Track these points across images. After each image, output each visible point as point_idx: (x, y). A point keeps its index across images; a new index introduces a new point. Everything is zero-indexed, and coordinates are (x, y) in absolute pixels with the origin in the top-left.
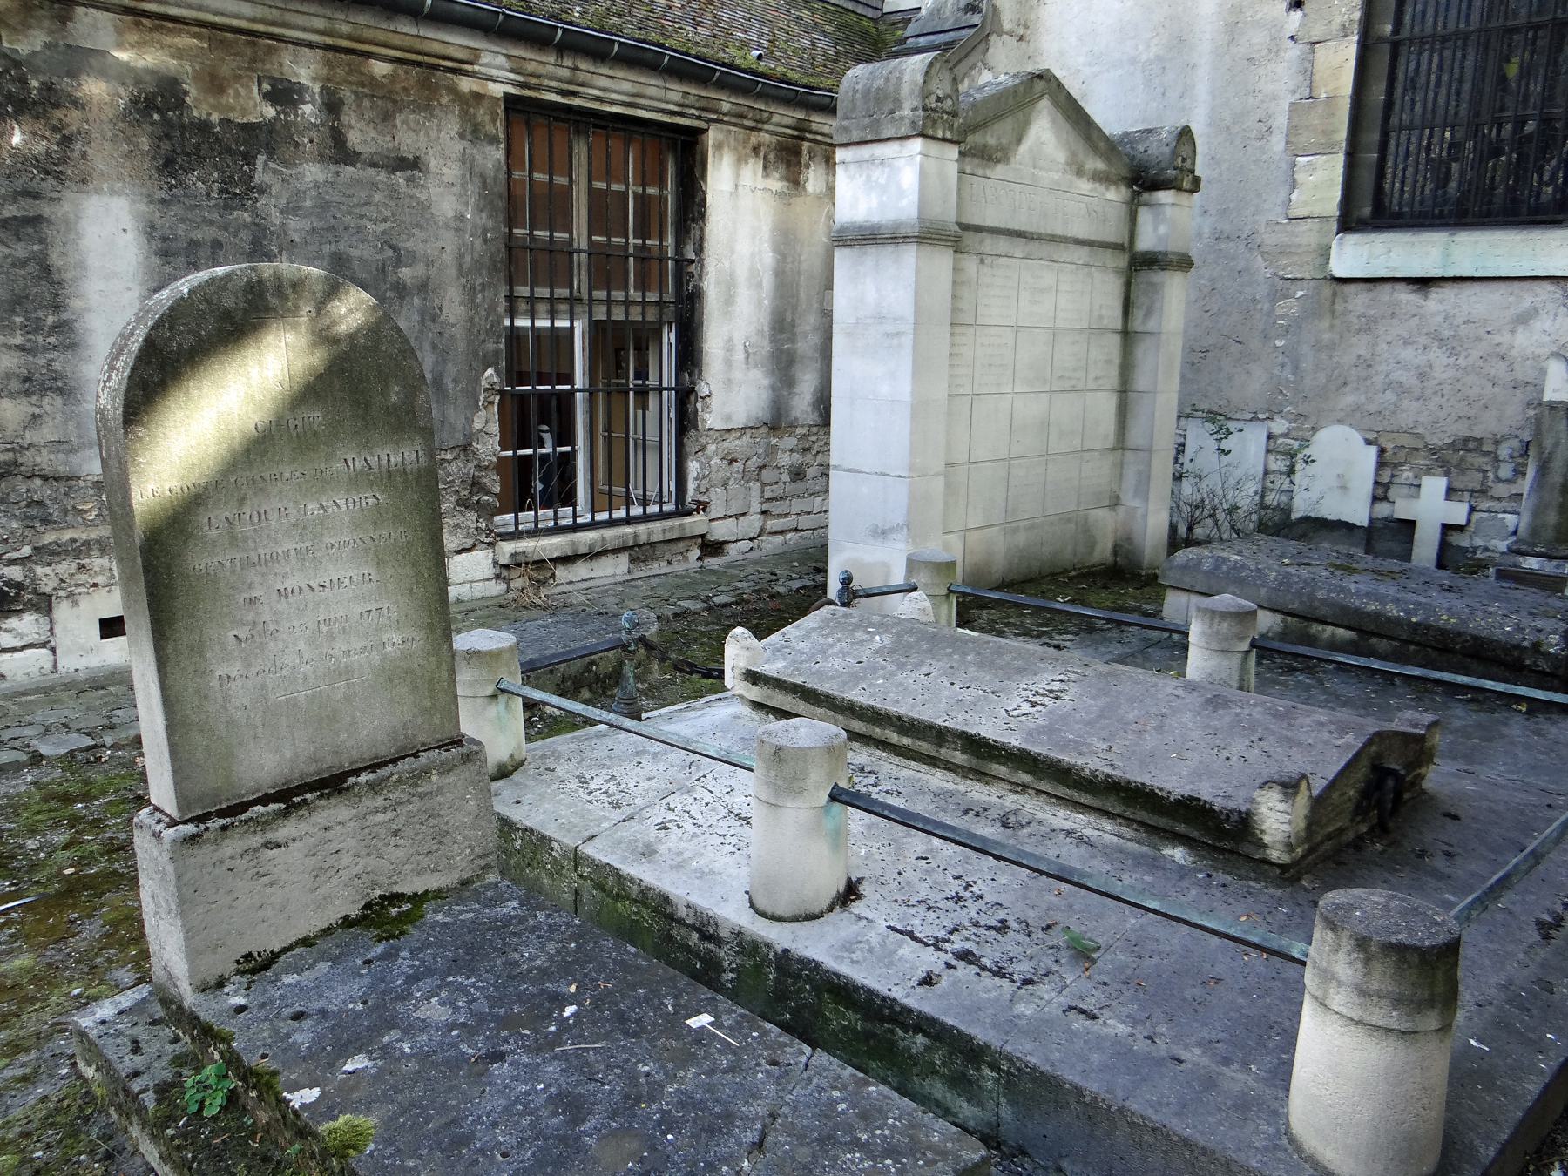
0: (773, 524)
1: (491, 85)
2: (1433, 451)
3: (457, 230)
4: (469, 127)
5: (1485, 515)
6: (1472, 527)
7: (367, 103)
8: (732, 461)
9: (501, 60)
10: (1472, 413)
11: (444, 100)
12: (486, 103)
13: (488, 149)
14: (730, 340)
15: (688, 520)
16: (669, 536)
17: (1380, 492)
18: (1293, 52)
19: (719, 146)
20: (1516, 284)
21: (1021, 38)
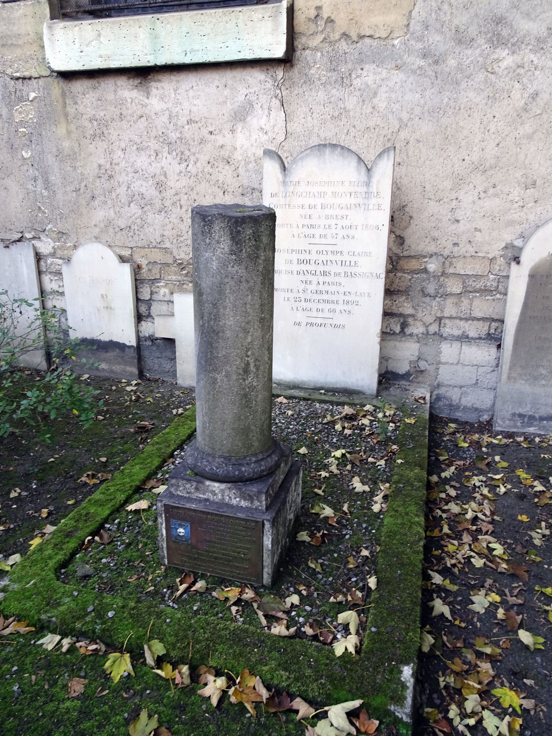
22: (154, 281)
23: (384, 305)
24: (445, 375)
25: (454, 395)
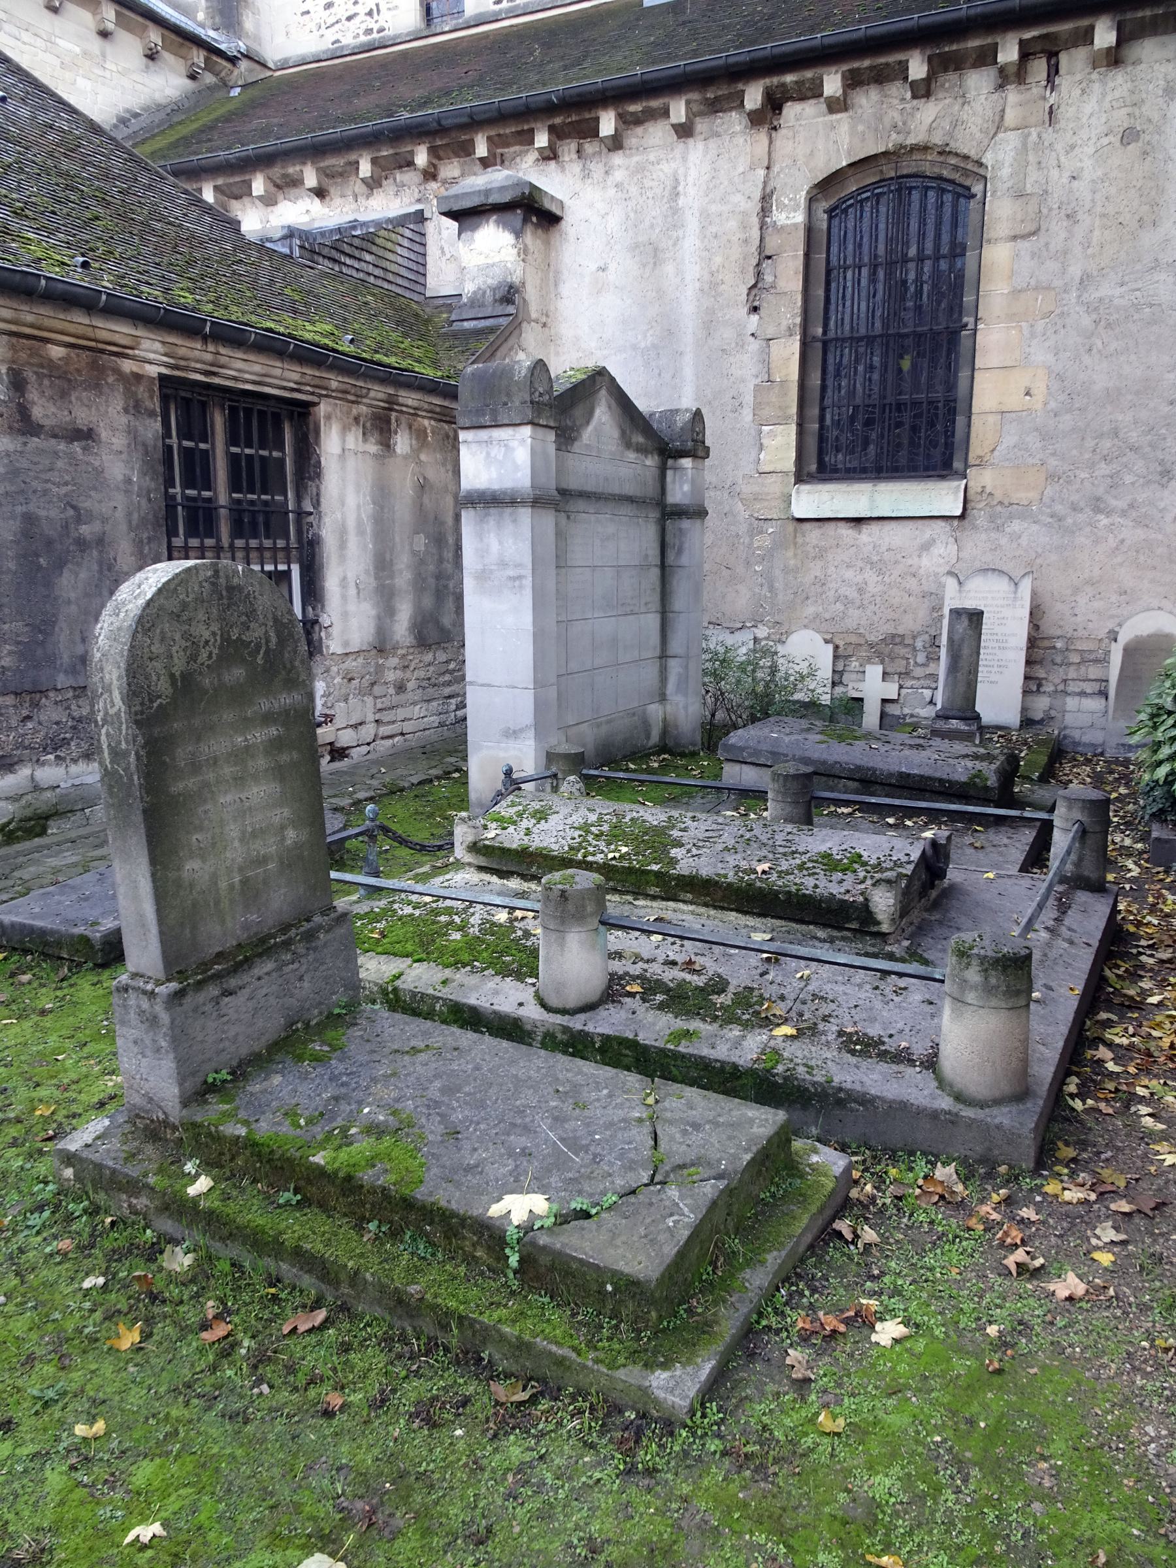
0: (384, 730)
1: (147, 366)
2: (871, 646)
3: (126, 491)
4: (132, 403)
7: (46, 382)
8: (350, 680)
9: (157, 346)
10: (896, 616)
11: (110, 380)
12: (144, 383)
13: (148, 421)
14: (345, 578)
17: (837, 678)
18: (754, 346)
19: (328, 417)
20: (920, 522)
21: (544, 325)
24: (1069, 720)
25: (1076, 735)
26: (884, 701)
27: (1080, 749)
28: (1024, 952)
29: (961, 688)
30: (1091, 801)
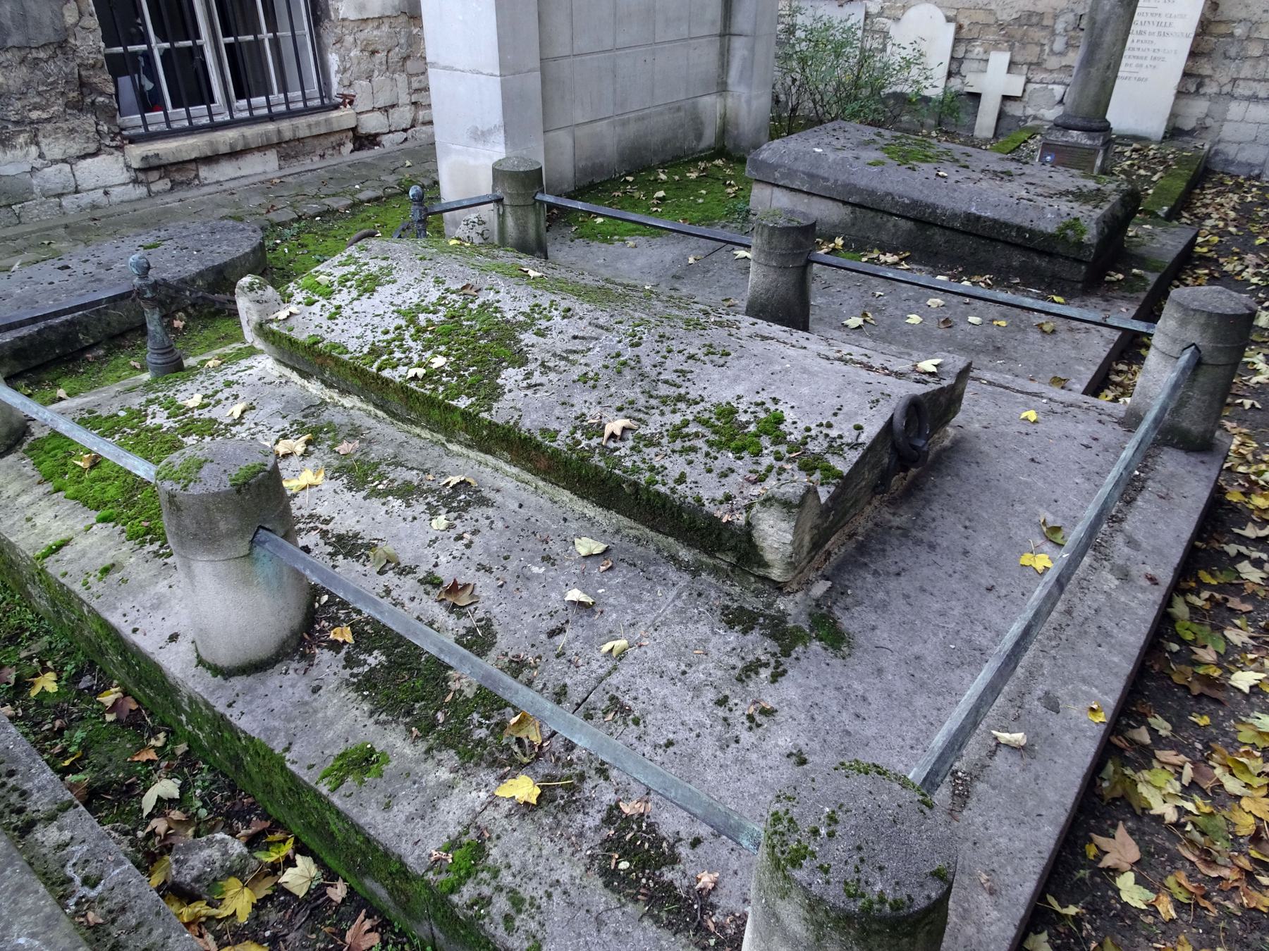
2: (1001, 27)
5: (1037, 86)
6: (1026, 99)
8: (373, 53)
15: (335, 114)
16: (315, 132)
22: (970, 41)
23: (1186, 66)
24: (1228, 131)
25: (1231, 150)
26: (1006, 98)
27: (1232, 169)
28: (923, 896)
29: (1092, 90)
30: (1223, 317)
